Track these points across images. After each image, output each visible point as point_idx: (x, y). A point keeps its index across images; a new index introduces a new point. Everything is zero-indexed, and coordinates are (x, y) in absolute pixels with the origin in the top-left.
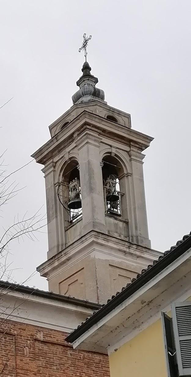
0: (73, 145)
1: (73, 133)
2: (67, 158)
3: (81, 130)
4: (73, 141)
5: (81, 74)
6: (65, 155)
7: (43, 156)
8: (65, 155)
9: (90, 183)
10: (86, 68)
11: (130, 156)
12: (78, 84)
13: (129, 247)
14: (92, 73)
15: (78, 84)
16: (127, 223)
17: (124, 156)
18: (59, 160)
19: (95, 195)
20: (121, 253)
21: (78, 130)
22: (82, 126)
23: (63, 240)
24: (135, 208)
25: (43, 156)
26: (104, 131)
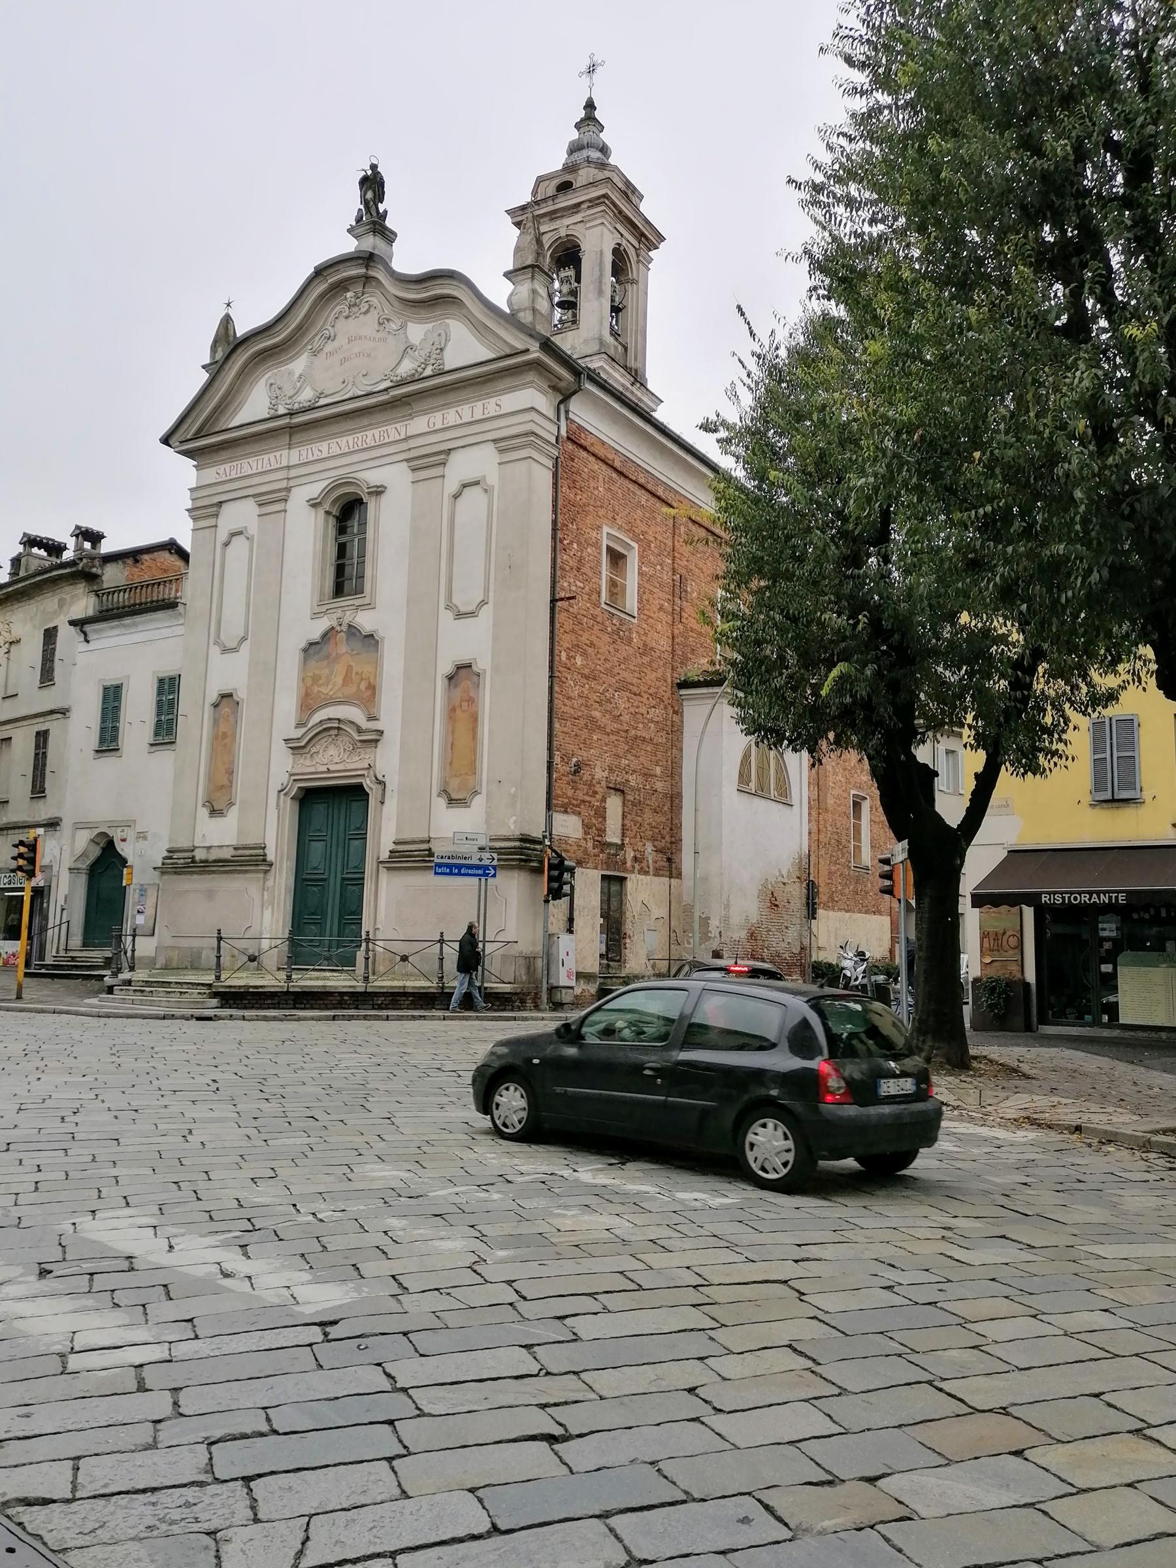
0: (578, 217)
1: (582, 202)
2: (563, 233)
3: (594, 202)
4: (576, 213)
5: (582, 114)
6: (564, 227)
7: (519, 216)
8: (564, 227)
9: (601, 282)
10: (590, 106)
11: (638, 256)
12: (578, 126)
13: (633, 384)
14: (597, 114)
15: (578, 126)
16: (626, 349)
17: (631, 252)
18: (365, 182)
19: (603, 301)
20: (234, 356)
21: (590, 201)
22: (598, 198)
23: (505, 341)
24: (637, 331)
25: (519, 216)
26: (620, 212)
